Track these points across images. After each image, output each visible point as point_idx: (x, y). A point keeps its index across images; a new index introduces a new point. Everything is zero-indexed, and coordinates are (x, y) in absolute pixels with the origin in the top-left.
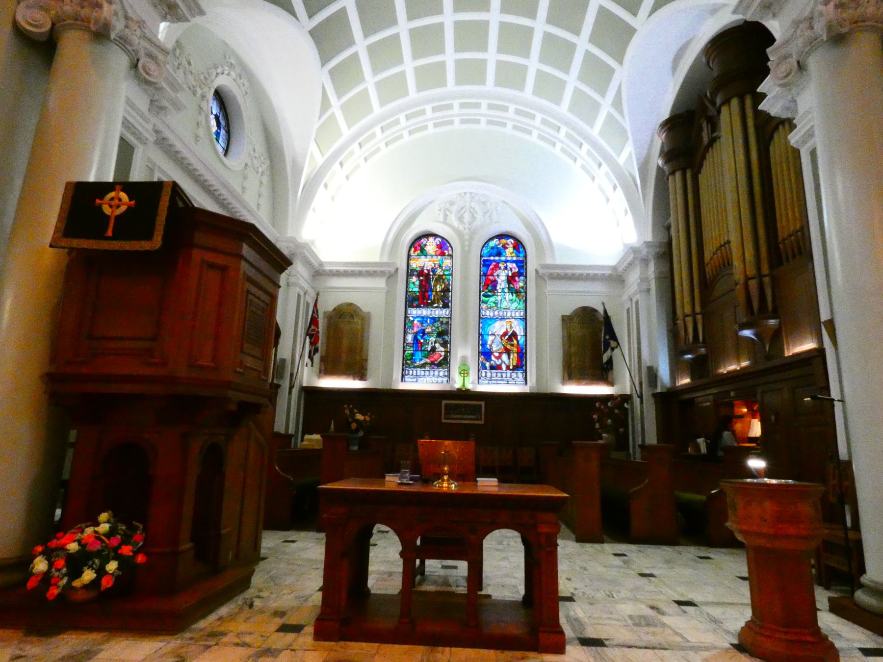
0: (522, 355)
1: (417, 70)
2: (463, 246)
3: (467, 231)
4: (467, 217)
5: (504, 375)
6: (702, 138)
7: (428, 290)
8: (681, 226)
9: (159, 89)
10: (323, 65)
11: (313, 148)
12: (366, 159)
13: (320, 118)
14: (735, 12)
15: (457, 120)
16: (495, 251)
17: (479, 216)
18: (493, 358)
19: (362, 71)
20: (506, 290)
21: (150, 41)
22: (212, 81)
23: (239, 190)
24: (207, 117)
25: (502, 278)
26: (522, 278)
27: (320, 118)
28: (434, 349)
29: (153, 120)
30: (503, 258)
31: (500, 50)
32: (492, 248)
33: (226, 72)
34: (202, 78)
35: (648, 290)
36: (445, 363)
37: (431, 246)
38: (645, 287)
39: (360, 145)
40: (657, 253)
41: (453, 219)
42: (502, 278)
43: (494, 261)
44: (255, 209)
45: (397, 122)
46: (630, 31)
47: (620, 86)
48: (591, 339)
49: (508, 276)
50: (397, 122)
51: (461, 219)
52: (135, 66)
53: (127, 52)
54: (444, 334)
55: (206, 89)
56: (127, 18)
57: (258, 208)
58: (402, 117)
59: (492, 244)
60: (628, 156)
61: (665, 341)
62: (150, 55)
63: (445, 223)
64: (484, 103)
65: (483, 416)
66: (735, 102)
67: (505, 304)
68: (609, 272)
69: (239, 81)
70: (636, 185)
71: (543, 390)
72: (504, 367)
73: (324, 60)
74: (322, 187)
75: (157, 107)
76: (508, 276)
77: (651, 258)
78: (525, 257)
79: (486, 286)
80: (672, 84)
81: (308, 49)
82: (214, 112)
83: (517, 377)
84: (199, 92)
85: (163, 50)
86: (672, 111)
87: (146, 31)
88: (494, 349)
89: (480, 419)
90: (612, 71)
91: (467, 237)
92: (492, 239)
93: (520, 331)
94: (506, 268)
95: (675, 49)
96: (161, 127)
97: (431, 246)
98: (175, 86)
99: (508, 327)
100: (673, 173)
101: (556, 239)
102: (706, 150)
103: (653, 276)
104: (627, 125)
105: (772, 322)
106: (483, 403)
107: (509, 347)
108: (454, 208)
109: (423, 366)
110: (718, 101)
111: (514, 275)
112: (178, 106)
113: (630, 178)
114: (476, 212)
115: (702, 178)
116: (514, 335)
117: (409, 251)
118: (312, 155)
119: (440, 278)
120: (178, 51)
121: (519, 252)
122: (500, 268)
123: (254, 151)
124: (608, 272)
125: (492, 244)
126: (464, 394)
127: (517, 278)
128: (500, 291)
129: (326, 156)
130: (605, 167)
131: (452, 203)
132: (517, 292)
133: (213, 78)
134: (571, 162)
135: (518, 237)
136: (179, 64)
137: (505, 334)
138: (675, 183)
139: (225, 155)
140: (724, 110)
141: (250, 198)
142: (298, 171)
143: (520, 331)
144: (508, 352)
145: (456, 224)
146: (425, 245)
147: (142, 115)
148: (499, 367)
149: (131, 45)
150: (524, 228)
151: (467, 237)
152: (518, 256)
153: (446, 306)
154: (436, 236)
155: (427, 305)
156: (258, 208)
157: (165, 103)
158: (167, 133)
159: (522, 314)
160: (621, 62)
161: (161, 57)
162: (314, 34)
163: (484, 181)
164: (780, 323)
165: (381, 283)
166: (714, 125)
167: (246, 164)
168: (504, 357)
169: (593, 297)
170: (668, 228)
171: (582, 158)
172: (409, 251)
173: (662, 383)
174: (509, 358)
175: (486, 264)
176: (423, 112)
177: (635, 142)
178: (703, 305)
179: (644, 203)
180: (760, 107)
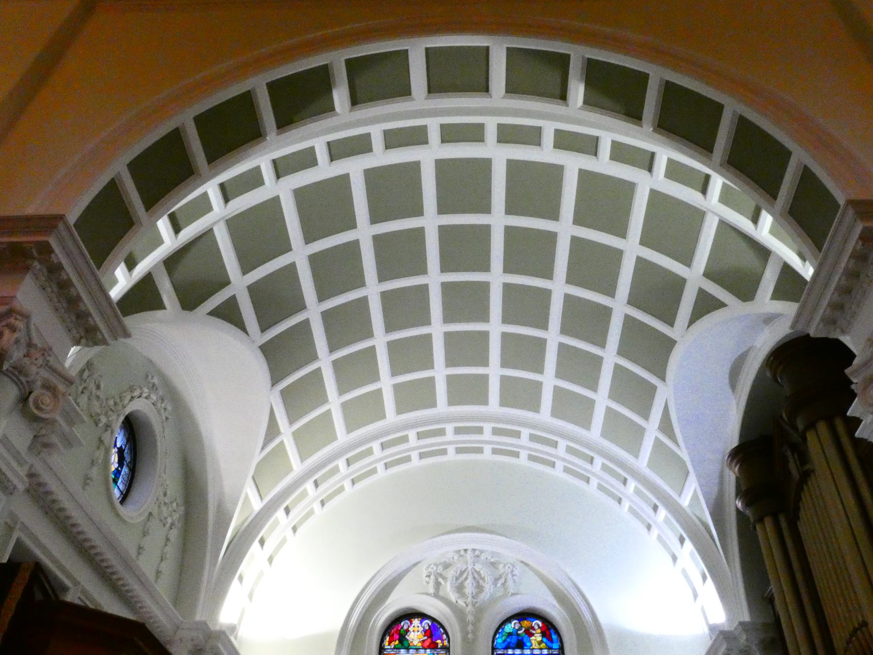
1: (397, 388)
2: (465, 633)
3: (470, 608)
4: (469, 588)
6: (790, 473)
8: (789, 598)
9: (50, 423)
10: (273, 385)
11: (250, 490)
12: (323, 503)
13: (263, 448)
14: (792, 327)
15: (451, 449)
16: (514, 639)
17: (488, 588)
19: (324, 387)
21: (54, 370)
22: (124, 407)
23: (133, 552)
24: (107, 453)
27: (263, 448)
29: (31, 459)
31: (506, 320)
32: (510, 634)
33: (145, 395)
34: (111, 402)
37: (416, 633)
39: (316, 484)
40: (762, 642)
44: (153, 581)
45: (370, 452)
46: (672, 343)
47: (666, 404)
50: (370, 452)
51: (460, 589)
52: (24, 400)
53: (18, 383)
55: (113, 417)
56: (30, 345)
57: (157, 577)
58: (376, 446)
59: (509, 628)
60: (691, 495)
62: (48, 387)
63: (436, 595)
64: (488, 427)
66: (822, 427)
69: (159, 405)
70: (714, 540)
73: (275, 380)
74: (256, 544)
75: (40, 445)
77: (754, 648)
80: (734, 402)
81: (259, 368)
82: (118, 445)
84: (104, 420)
85: (66, 379)
86: (742, 436)
87: (51, 359)
90: (654, 388)
91: (470, 618)
92: (508, 620)
95: (731, 357)
96: (39, 468)
97: (416, 633)
98: (72, 419)
100: (761, 520)
102: (800, 488)
104: (684, 454)
108: (451, 573)
110: (800, 426)
112: (69, 442)
113: (702, 528)
114: (483, 579)
115: (802, 527)
117: (382, 641)
118: (247, 498)
120: (86, 374)
121: (551, 641)
123: (165, 494)
125: (509, 628)
129: (267, 499)
130: (663, 513)
131: (447, 566)
133: (126, 402)
134: (612, 503)
136: (85, 388)
138: (766, 532)
139: (122, 502)
140: (811, 437)
141: (147, 565)
142: (224, 520)
145: (453, 597)
146: (407, 631)
147: (17, 456)
149: (26, 375)
150: (555, 603)
151: (470, 618)
152: (550, 648)
154: (423, 616)
156: (157, 577)
157: (54, 439)
158: (45, 477)
160: (663, 378)
161: (61, 387)
162: (266, 350)
163: (492, 532)
166: (803, 457)
167: (150, 514)
170: (771, 600)
171: (628, 497)
172: (382, 641)
176: (405, 439)
177: (699, 477)
180: (857, 434)
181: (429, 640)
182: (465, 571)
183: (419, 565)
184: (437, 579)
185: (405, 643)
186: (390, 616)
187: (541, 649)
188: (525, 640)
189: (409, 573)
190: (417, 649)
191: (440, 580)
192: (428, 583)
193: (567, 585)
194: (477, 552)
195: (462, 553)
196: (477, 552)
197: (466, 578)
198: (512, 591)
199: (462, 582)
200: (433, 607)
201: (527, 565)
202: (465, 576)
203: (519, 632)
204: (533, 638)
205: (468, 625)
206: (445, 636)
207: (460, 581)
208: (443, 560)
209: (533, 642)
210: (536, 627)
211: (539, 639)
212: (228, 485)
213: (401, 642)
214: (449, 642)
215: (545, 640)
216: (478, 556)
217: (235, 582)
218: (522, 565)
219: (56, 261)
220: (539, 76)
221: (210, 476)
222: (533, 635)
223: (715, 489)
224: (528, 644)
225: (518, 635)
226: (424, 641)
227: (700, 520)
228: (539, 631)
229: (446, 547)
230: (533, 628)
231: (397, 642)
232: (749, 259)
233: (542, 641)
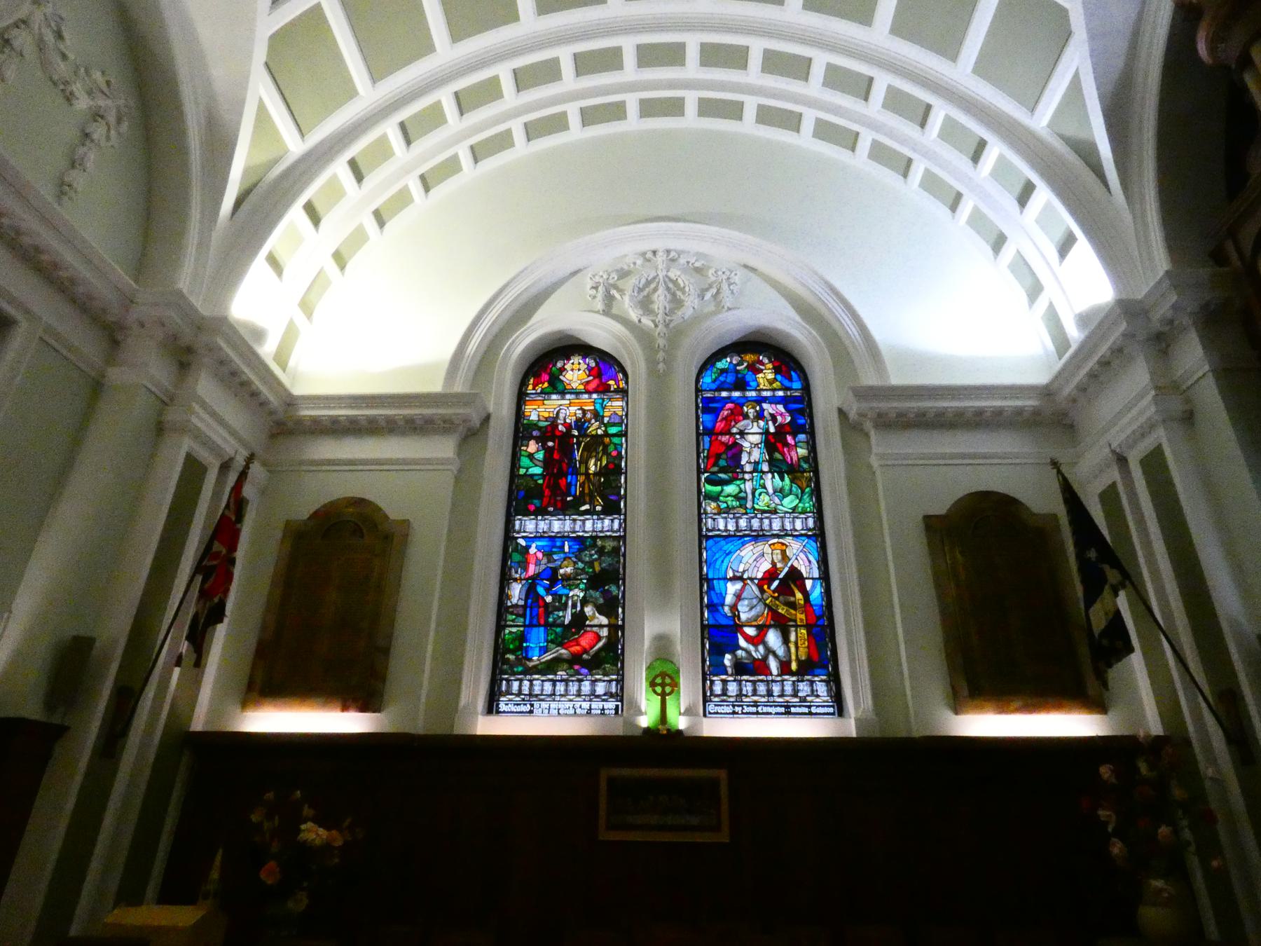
0: (822, 630)
2: (652, 363)
4: (660, 300)
5: (776, 689)
7: (568, 470)
16: (730, 379)
20: (765, 467)
28: (580, 620)
35: (1189, 418)
36: (609, 658)
38: (1176, 406)
41: (628, 306)
43: (729, 399)
44: (47, 192)
51: (645, 305)
54: (606, 578)
63: (607, 312)
72: (773, 665)
77: (1186, 321)
78: (807, 388)
79: (714, 457)
88: (744, 617)
89: (717, 828)
91: (661, 342)
93: (807, 565)
107: (782, 610)
109: (549, 668)
111: (781, 430)
114: (683, 290)
116: (795, 577)
119: (596, 444)
126: (664, 745)
127: (789, 439)
130: (996, 150)
131: (624, 274)
132: (792, 471)
137: (771, 575)
142: (220, 147)
143: (807, 565)
144: (783, 626)
145: (634, 315)
148: (759, 667)
152: (785, 389)
153: (611, 509)
154: (585, 350)
155: (566, 508)
165: (443, 448)
168: (773, 638)
174: (786, 641)
175: (708, 406)
179: (1128, 197)
181: (597, 381)
182: (654, 278)
183: (579, 275)
184: (608, 291)
185: (560, 387)
186: (534, 343)
189: (563, 288)
190: (578, 393)
191: (614, 292)
192: (594, 297)
193: (819, 289)
194: (673, 254)
195: (649, 255)
196: (673, 254)
197: (655, 290)
198: (728, 305)
199: (648, 296)
200: (600, 332)
201: (753, 270)
202: (653, 286)
204: (760, 375)
205: (657, 352)
206: (620, 376)
207: (645, 293)
208: (619, 266)
209: (761, 381)
211: (771, 376)
212: (219, 73)
213: (552, 384)
214: (627, 383)
215: (779, 377)
216: (673, 260)
217: (258, 267)
218: (746, 271)
221: (174, 32)
223: (1119, 63)
225: (737, 372)
226: (588, 382)
229: (623, 245)
231: (546, 385)
233: (775, 380)
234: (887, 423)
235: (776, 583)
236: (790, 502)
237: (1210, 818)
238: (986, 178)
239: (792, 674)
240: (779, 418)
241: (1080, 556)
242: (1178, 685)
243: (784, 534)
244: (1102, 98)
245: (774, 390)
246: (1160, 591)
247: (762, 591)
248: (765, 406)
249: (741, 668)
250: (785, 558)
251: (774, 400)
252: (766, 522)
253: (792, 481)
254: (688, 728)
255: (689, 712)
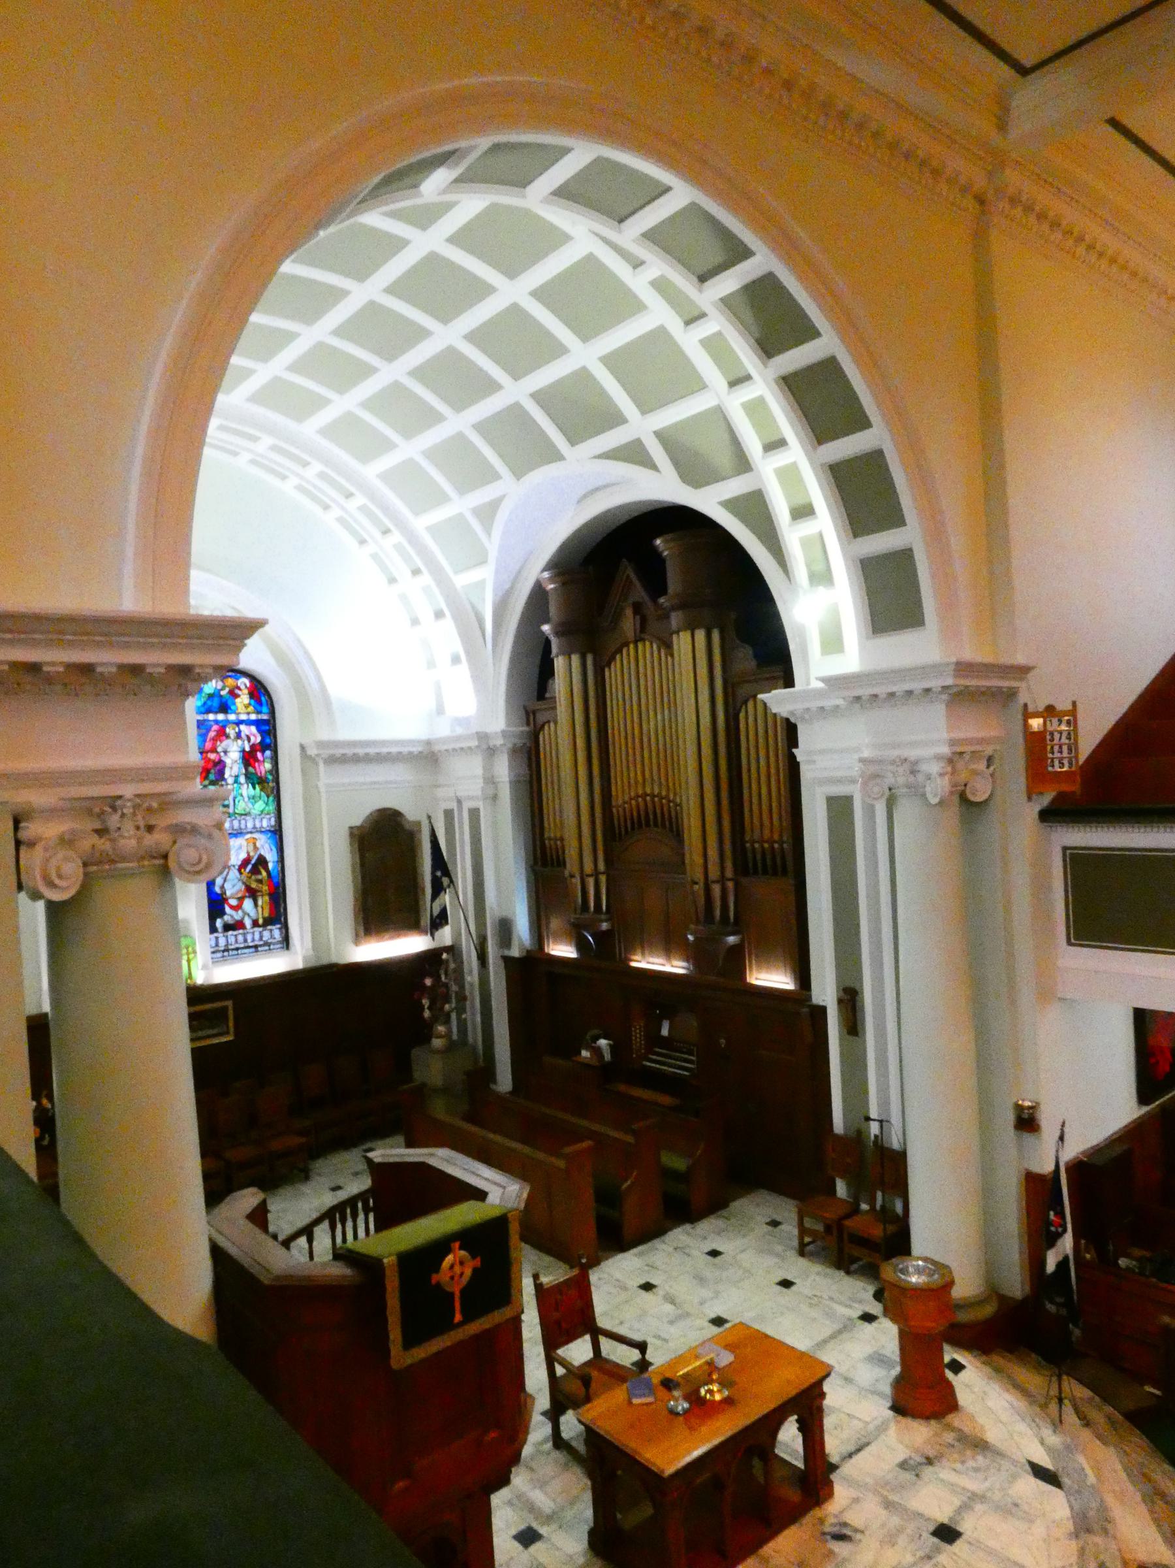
5: (249, 938)
16: (215, 703)
18: (227, 909)
20: (242, 779)
25: (232, 754)
26: (268, 753)
30: (232, 717)
35: (495, 798)
38: (491, 792)
42: (232, 754)
43: (216, 722)
48: (392, 865)
49: (243, 751)
61: (523, 878)
65: (231, 1024)
67: (241, 807)
68: (420, 749)
71: (325, 961)
72: (248, 923)
76: (243, 751)
77: (505, 750)
78: (272, 712)
83: (272, 937)
88: (228, 893)
89: (228, 1033)
93: (271, 857)
94: (239, 736)
99: (251, 848)
101: (335, 690)
103: (507, 779)
105: (732, 939)
106: (229, 1003)
107: (254, 885)
111: (254, 748)
113: (472, 615)
116: (262, 861)
121: (261, 704)
122: (228, 737)
124: (416, 749)
127: (259, 755)
128: (230, 780)
132: (261, 781)
135: (254, 674)
137: (246, 862)
143: (271, 857)
144: (252, 893)
148: (238, 925)
159: (273, 822)
164: (742, 940)
168: (248, 904)
169: (393, 790)
173: (520, 939)
174: (256, 905)
178: (608, 861)
179: (494, 656)
187: (248, 713)
188: (229, 702)
203: (223, 693)
210: (243, 687)
219: (162, 670)
220: (704, 249)
222: (237, 696)
224: (233, 707)
227: (473, 607)
228: (246, 691)
230: (239, 688)
232: (723, 459)
234: (332, 760)
235: (250, 867)
236: (260, 805)
237: (465, 998)
238: (420, 591)
239: (259, 926)
240: (253, 739)
241: (433, 873)
242: (463, 931)
243: (255, 830)
244: (494, 603)
245: (248, 713)
246: (465, 894)
247: (241, 873)
248: (242, 727)
249: (227, 927)
250: (256, 848)
251: (249, 723)
252: (243, 822)
253: (261, 790)
254: (829, 1407)
255: (205, 967)
